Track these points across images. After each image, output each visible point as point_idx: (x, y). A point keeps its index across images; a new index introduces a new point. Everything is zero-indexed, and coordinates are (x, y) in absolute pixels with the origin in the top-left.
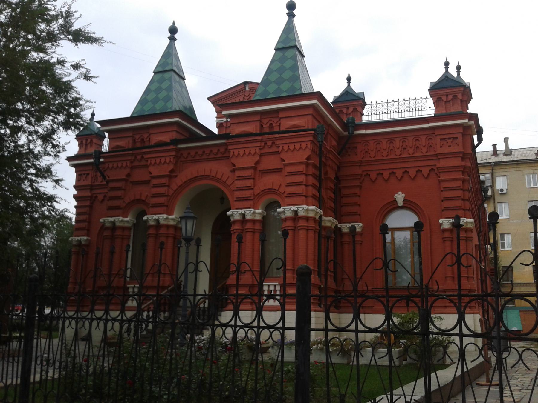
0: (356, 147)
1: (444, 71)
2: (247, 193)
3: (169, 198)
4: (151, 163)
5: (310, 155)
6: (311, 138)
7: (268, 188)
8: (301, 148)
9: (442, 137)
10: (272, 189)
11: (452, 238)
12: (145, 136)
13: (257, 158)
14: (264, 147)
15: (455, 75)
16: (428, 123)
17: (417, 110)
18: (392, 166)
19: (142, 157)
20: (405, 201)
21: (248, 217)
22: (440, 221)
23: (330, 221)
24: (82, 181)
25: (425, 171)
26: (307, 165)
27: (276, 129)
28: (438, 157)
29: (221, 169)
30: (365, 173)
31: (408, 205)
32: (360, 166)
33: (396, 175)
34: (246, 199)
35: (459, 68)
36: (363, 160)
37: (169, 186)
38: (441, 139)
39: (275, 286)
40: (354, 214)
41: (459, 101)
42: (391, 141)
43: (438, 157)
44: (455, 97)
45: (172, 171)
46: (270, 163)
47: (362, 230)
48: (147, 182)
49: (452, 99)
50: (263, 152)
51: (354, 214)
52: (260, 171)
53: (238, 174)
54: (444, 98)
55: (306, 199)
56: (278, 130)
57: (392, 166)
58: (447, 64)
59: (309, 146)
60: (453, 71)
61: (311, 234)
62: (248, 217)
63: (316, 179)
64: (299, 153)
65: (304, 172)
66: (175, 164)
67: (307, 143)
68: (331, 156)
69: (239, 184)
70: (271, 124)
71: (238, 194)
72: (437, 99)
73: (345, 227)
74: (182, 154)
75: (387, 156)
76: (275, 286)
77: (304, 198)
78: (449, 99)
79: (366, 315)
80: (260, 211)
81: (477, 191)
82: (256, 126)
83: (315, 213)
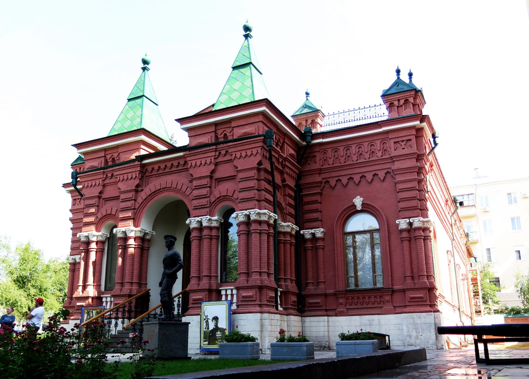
0: (315, 156)
1: (396, 78)
2: (204, 201)
3: (135, 211)
4: (120, 180)
5: (261, 161)
6: (261, 144)
7: (223, 195)
8: (252, 154)
9: (396, 140)
10: (226, 196)
11: (410, 238)
12: (115, 155)
13: (212, 167)
14: (219, 156)
15: (407, 81)
16: (381, 127)
17: (372, 117)
18: (350, 172)
19: (112, 175)
20: (363, 204)
21: (205, 224)
22: (397, 222)
23: (288, 226)
24: (76, 205)
25: (382, 174)
26: (259, 170)
27: (230, 138)
28: (392, 160)
29: (179, 180)
30: (325, 180)
31: (366, 209)
32: (319, 174)
33: (354, 180)
34: (202, 207)
35: (410, 75)
36: (323, 167)
37: (135, 200)
38: (395, 143)
39: (232, 290)
40: (316, 220)
41: (411, 105)
42: (348, 148)
43: (392, 160)
44: (406, 101)
45: (137, 186)
46: (224, 171)
47: (324, 235)
48: (117, 198)
49: (404, 103)
50: (217, 161)
51: (316, 220)
52: (216, 179)
53: (195, 183)
54: (396, 103)
55: (259, 202)
56: (232, 138)
57: (350, 172)
58: (398, 72)
59: (259, 151)
60: (404, 78)
61: (265, 237)
62: (205, 224)
63: (270, 184)
64: (250, 159)
65: (255, 177)
66: (141, 179)
67: (257, 149)
68: (287, 164)
69: (196, 193)
70: (225, 135)
71: (195, 203)
72: (390, 104)
73: (307, 233)
74: (147, 170)
75: (345, 162)
76: (232, 290)
77: (257, 202)
78: (401, 104)
79: (331, 318)
80: (216, 218)
81: (447, 201)
82: (211, 137)
83: (267, 216)
